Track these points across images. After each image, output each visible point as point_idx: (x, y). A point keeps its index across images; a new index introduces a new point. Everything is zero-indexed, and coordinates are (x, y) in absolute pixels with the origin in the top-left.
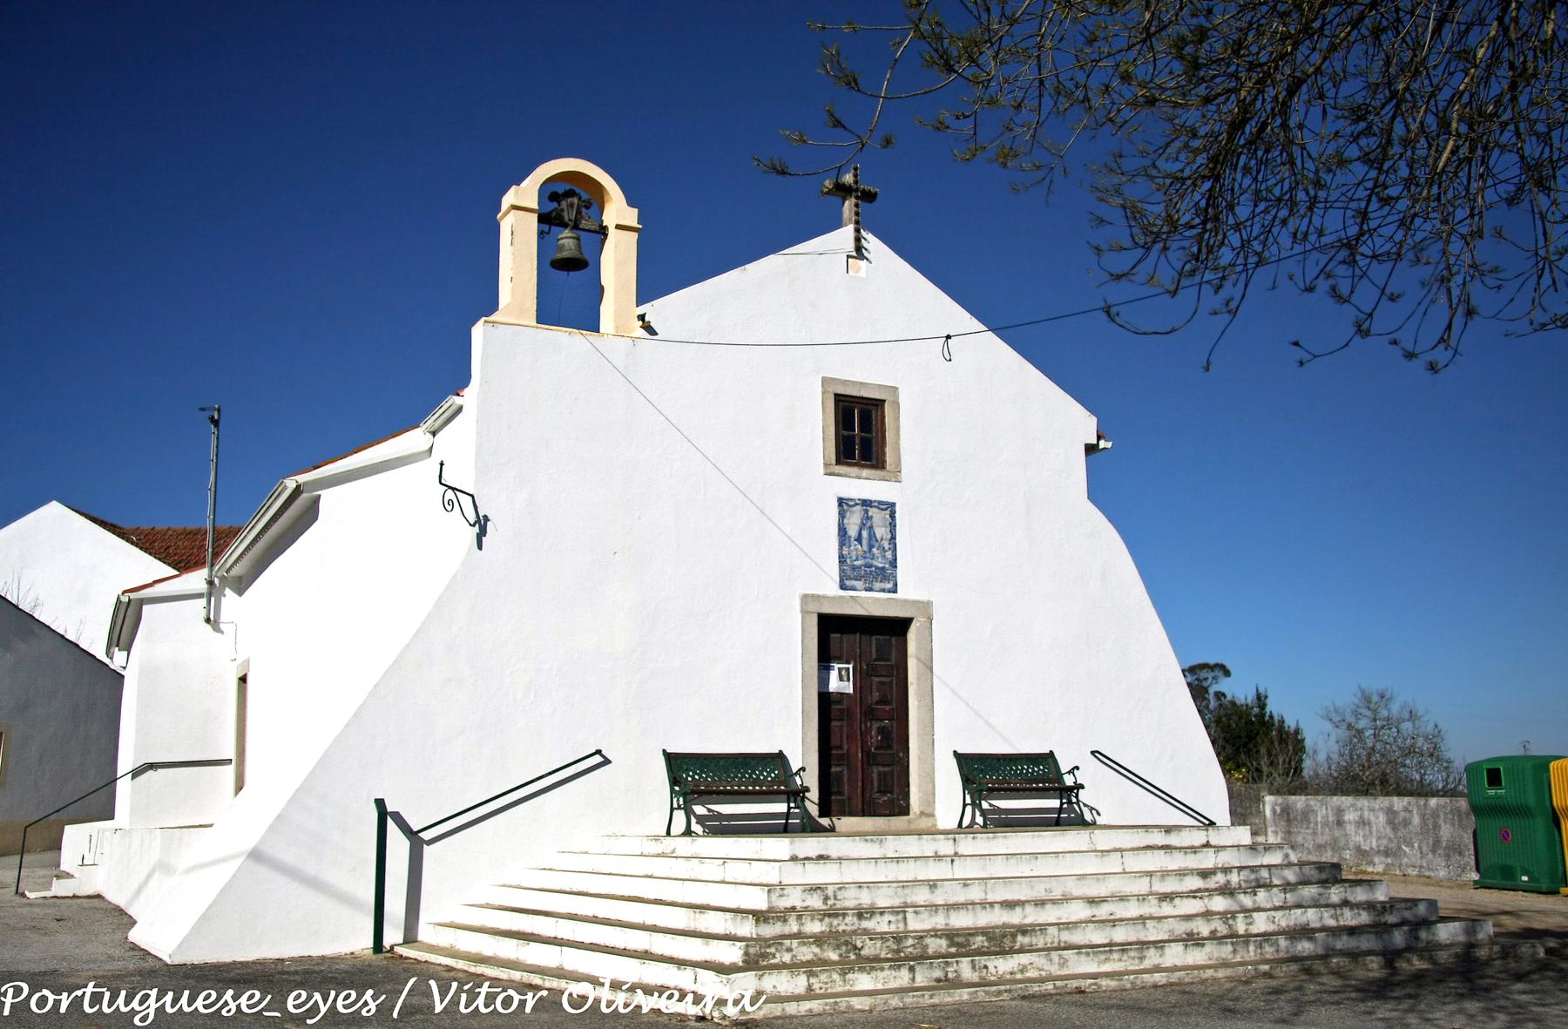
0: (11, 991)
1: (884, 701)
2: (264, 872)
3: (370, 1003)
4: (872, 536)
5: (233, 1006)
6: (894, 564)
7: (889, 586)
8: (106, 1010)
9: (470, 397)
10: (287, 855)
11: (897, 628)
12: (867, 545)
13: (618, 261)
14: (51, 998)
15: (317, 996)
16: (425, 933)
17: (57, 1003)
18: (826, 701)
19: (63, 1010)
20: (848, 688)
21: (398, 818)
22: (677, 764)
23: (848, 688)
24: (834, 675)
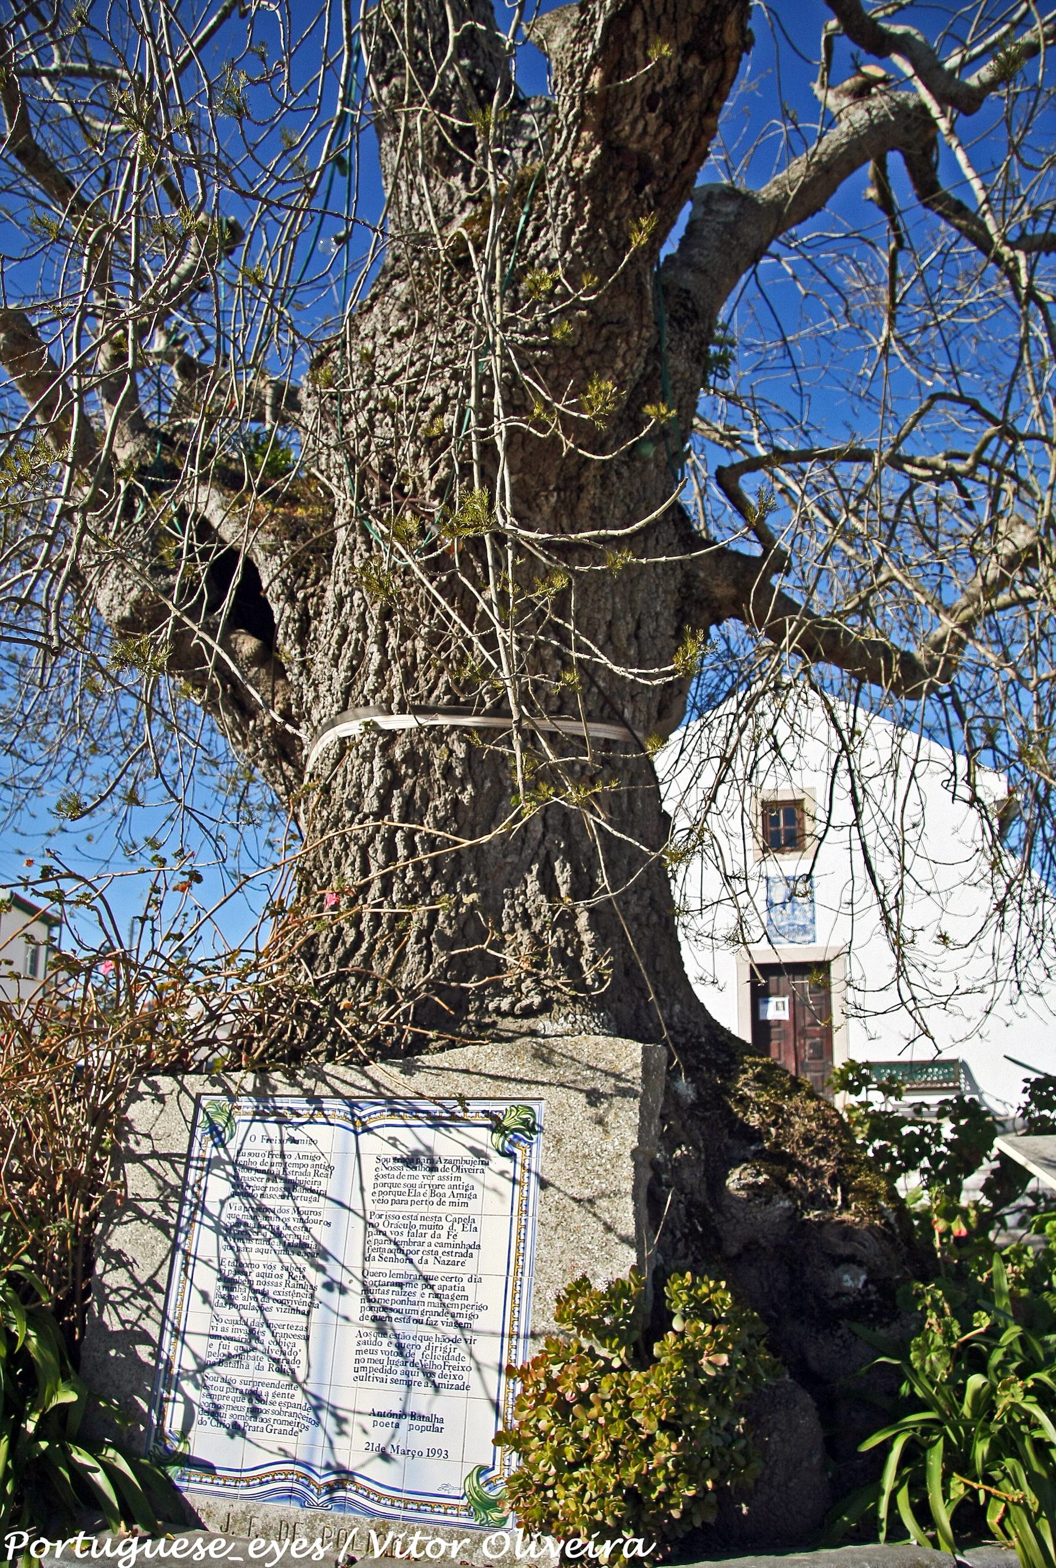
0: (13, 1540)
5: (202, 1552)
6: (813, 921)
7: (809, 938)
14: (444, 1544)
15: (274, 1544)
20: (785, 1015)
23: (785, 1015)
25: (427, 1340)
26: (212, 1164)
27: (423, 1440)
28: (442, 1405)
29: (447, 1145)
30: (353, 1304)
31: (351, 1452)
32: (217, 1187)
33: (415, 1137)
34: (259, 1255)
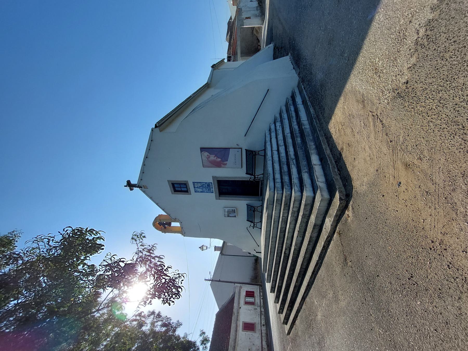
12: (205, 187)
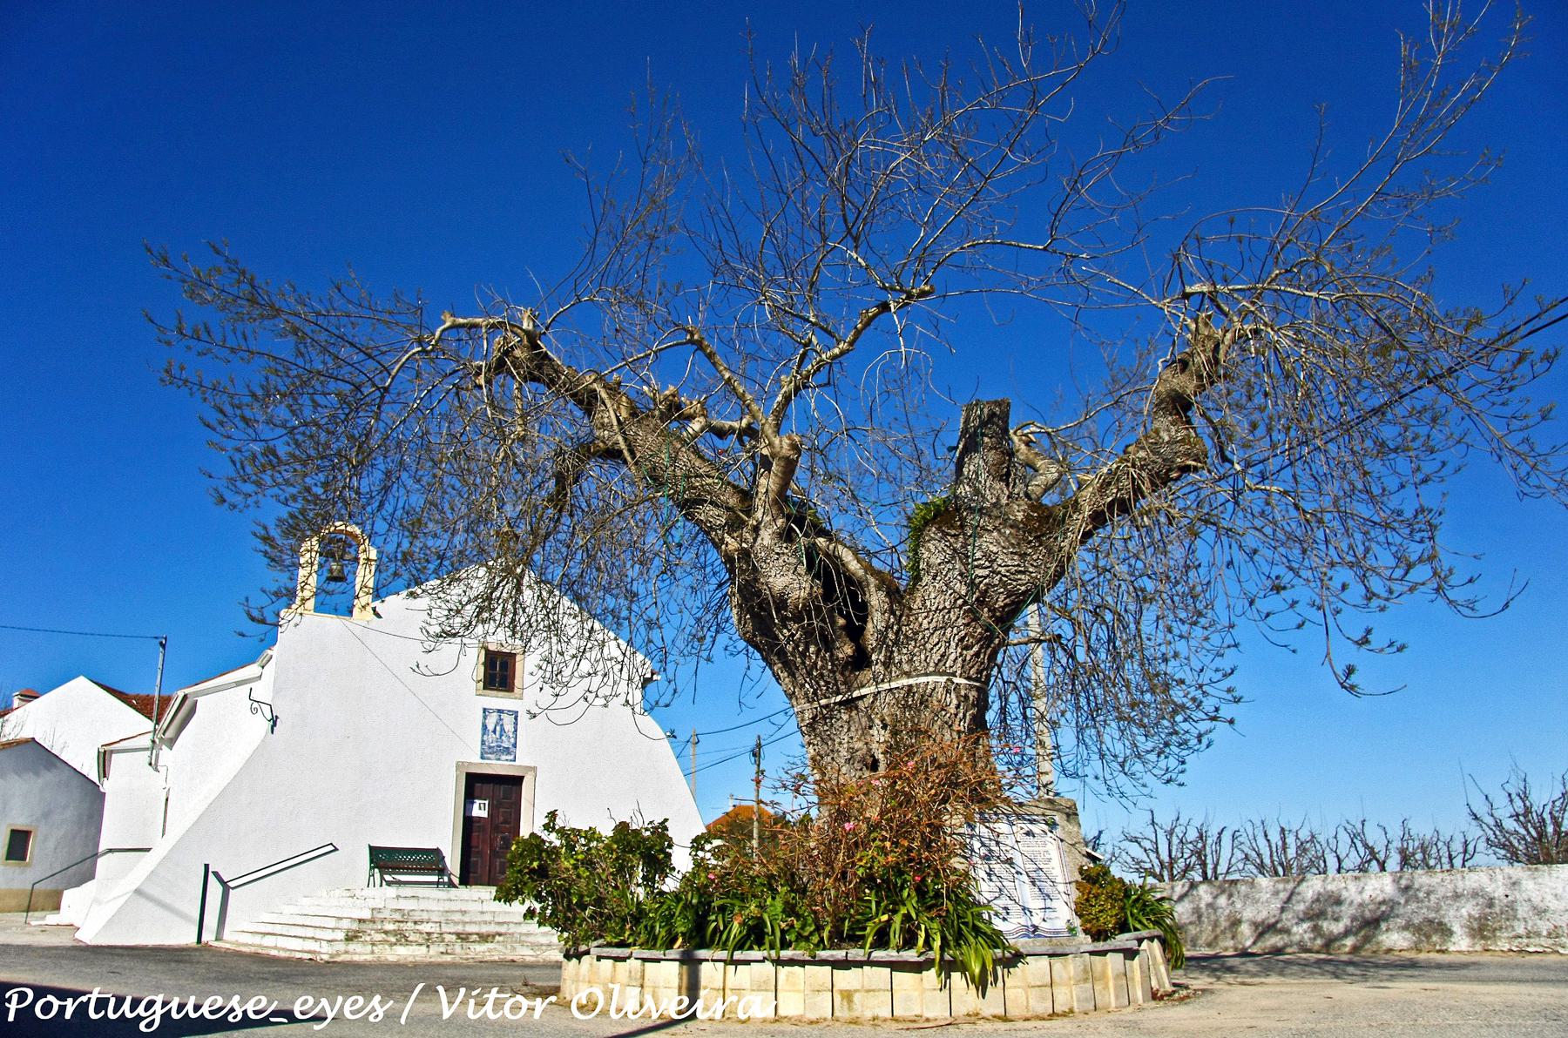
1: (505, 822)
2: (142, 901)
3: (378, 1007)
4: (502, 730)
5: (239, 1013)
6: (515, 746)
8: (111, 1016)
9: (275, 652)
10: (154, 891)
11: (517, 781)
12: (498, 739)
13: (364, 576)
14: (56, 1003)
15: (324, 1002)
16: (227, 935)
17: (62, 1009)
18: (469, 823)
19: (68, 1016)
21: (216, 874)
22: (374, 851)
23: (484, 814)
24: (476, 806)
25: (1048, 889)
26: (972, 837)
27: (1053, 915)
28: (1053, 904)
29: (1035, 829)
30: (1024, 878)
31: (1036, 921)
32: (977, 845)
33: (1028, 826)
34: (997, 868)
